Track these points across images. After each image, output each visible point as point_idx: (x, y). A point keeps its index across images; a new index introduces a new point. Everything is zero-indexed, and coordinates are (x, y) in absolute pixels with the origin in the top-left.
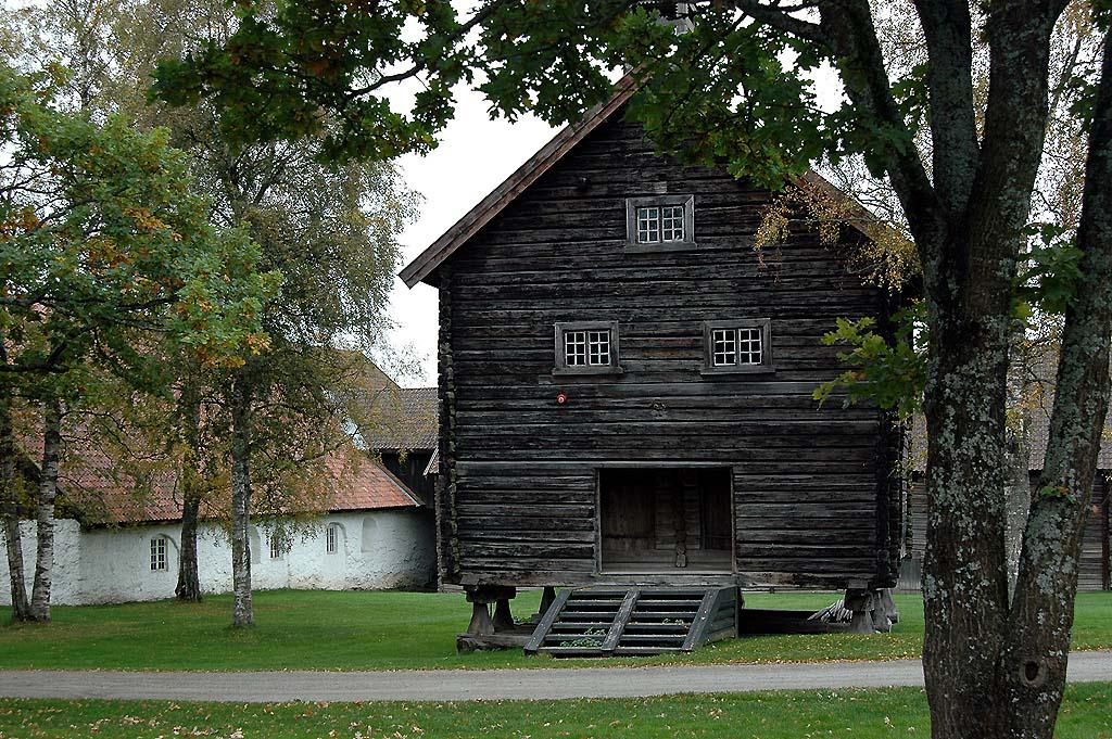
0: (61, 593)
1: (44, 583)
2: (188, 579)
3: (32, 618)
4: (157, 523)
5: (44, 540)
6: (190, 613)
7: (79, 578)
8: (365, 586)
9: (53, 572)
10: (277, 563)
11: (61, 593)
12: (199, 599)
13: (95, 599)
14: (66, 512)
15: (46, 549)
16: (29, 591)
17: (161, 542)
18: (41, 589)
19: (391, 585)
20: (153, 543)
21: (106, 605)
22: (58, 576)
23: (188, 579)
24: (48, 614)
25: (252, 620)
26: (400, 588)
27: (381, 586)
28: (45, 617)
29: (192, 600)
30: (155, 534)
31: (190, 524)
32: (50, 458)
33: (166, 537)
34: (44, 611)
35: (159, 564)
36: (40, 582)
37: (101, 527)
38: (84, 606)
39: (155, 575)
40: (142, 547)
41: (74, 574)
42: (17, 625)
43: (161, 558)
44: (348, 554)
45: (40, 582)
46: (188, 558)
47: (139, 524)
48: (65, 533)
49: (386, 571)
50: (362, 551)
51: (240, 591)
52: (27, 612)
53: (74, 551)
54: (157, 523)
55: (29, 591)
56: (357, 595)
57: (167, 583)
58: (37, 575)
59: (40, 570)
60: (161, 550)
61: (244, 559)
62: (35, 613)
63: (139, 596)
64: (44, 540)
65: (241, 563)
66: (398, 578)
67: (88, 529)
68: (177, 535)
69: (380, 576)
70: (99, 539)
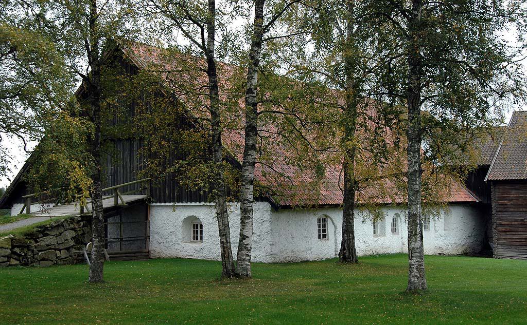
0: (259, 253)
1: (246, 248)
2: (349, 245)
3: (237, 275)
4: (322, 207)
5: (246, 214)
6: (347, 272)
7: (271, 243)
8: (446, 252)
9: (251, 241)
10: (395, 236)
11: (259, 253)
12: (356, 261)
13: (282, 259)
14: (260, 198)
15: (247, 221)
16: (235, 251)
17: (324, 220)
18: (244, 252)
19: (460, 252)
20: (319, 220)
21: (289, 263)
22: (256, 242)
23: (349, 245)
24: (249, 272)
25: (426, 286)
26: (465, 254)
27: (455, 252)
28: (247, 275)
29: (351, 262)
30: (320, 214)
31: (349, 208)
32: (249, 148)
33: (327, 216)
34: (247, 270)
35: (323, 235)
36: (242, 247)
37: (286, 208)
38: (275, 263)
39: (320, 242)
40: (311, 222)
41: (267, 241)
42: (226, 281)
43: (324, 231)
44: (436, 231)
45: (243, 246)
46: (348, 231)
47: (313, 206)
48: (261, 211)
49: (462, 244)
50: (444, 230)
51: (415, 259)
52: (233, 271)
53: (267, 225)
54: (322, 207)
55: (235, 251)
56: (440, 260)
57: (331, 247)
58: (241, 241)
59: (243, 237)
60: (324, 226)
61: (418, 231)
62: (240, 271)
63: (311, 257)
64: (246, 214)
65: (416, 234)
66: (464, 247)
67: (276, 208)
68: (338, 219)
69: (454, 246)
70: (284, 216)
